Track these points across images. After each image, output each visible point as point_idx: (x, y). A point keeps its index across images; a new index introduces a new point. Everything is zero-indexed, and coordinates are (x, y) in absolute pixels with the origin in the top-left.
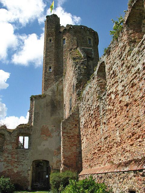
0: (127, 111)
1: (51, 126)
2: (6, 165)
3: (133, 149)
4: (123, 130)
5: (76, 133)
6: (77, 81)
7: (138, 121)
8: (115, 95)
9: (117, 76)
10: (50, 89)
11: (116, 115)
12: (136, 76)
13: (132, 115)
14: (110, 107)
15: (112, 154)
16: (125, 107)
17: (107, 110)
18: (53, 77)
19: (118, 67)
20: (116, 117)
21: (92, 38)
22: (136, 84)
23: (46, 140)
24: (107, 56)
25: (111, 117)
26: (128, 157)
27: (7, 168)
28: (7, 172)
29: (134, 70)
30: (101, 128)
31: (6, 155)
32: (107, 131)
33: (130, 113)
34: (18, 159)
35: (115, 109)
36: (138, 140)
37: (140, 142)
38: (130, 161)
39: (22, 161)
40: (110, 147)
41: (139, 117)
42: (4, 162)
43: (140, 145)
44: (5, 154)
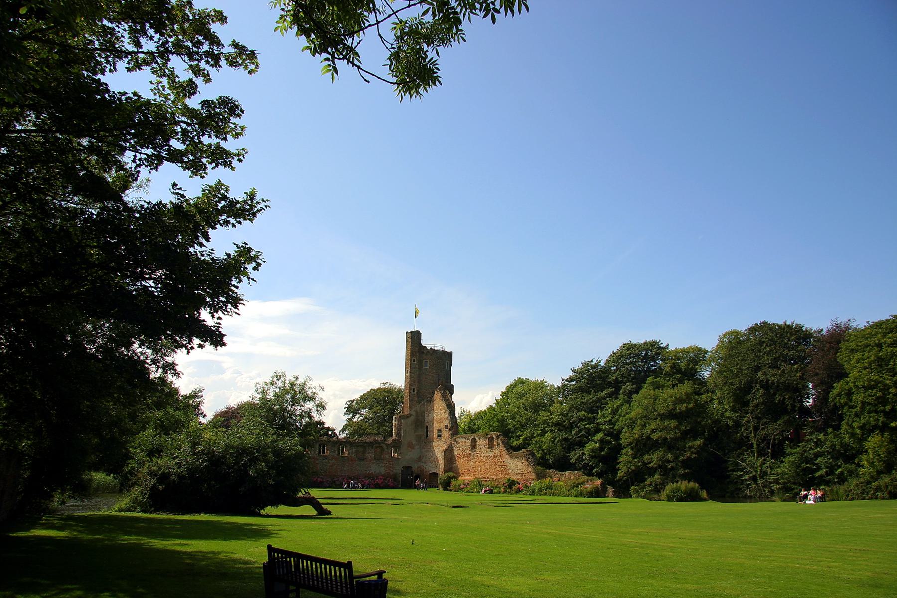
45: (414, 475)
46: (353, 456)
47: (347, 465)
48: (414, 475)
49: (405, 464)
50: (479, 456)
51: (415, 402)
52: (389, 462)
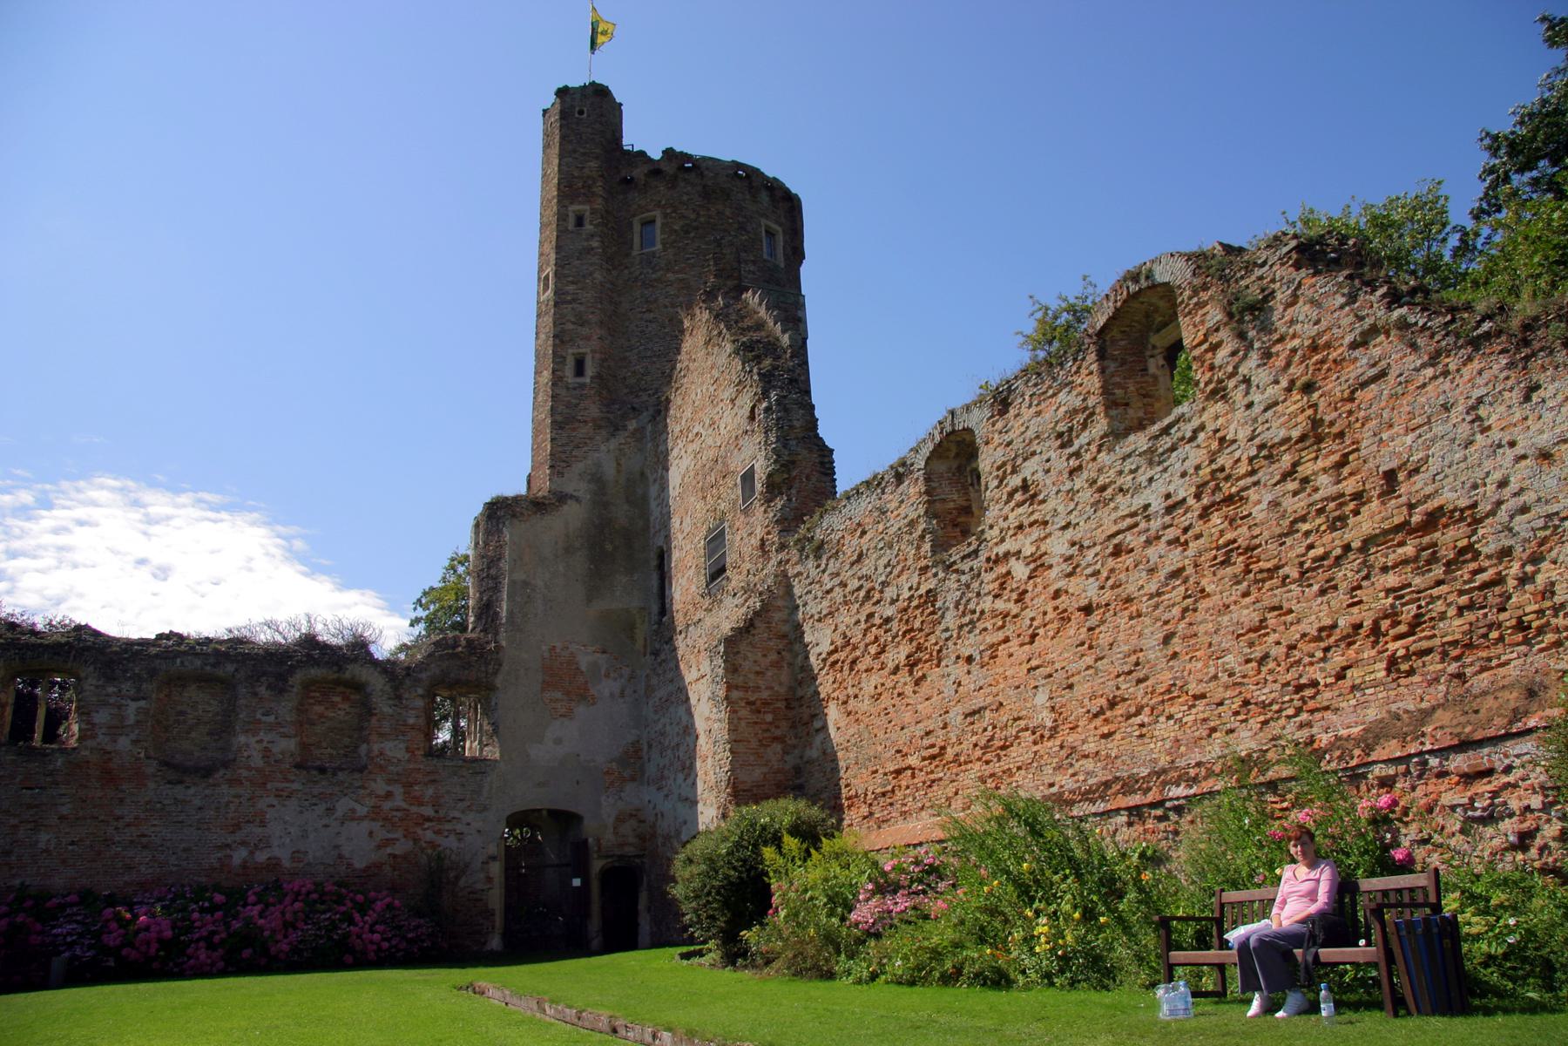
0: (1090, 629)
1: (590, 649)
2: (381, 834)
3: (1112, 747)
4: (1070, 687)
5: (782, 690)
6: (776, 462)
7: (1137, 664)
8: (1032, 566)
9: (1044, 501)
10: (579, 467)
11: (1034, 636)
12: (1136, 525)
13: (1111, 645)
14: (1000, 605)
15: (1009, 769)
16: (1080, 615)
17: (982, 612)
18: (594, 410)
19: (1048, 471)
20: (1032, 642)
21: (779, 229)
22: (1132, 550)
23: (568, 715)
24: (993, 416)
25: (1006, 640)
26: (1088, 773)
27: (389, 850)
28: (387, 869)
29: (1125, 504)
30: (949, 675)
31: (380, 786)
32: (981, 688)
33: (1101, 636)
34: (436, 803)
35: (1029, 613)
36: (1138, 720)
37: (1142, 725)
38: (1107, 785)
39: (457, 814)
40: (997, 743)
41: (1141, 650)
42: (373, 820)
43: (1141, 736)
44: (373, 784)
45: (597, 865)
46: (124, 743)
47: (65, 810)
48: (597, 865)
49: (530, 797)
50: (1020, 570)
51: (584, 430)
52: (408, 786)
